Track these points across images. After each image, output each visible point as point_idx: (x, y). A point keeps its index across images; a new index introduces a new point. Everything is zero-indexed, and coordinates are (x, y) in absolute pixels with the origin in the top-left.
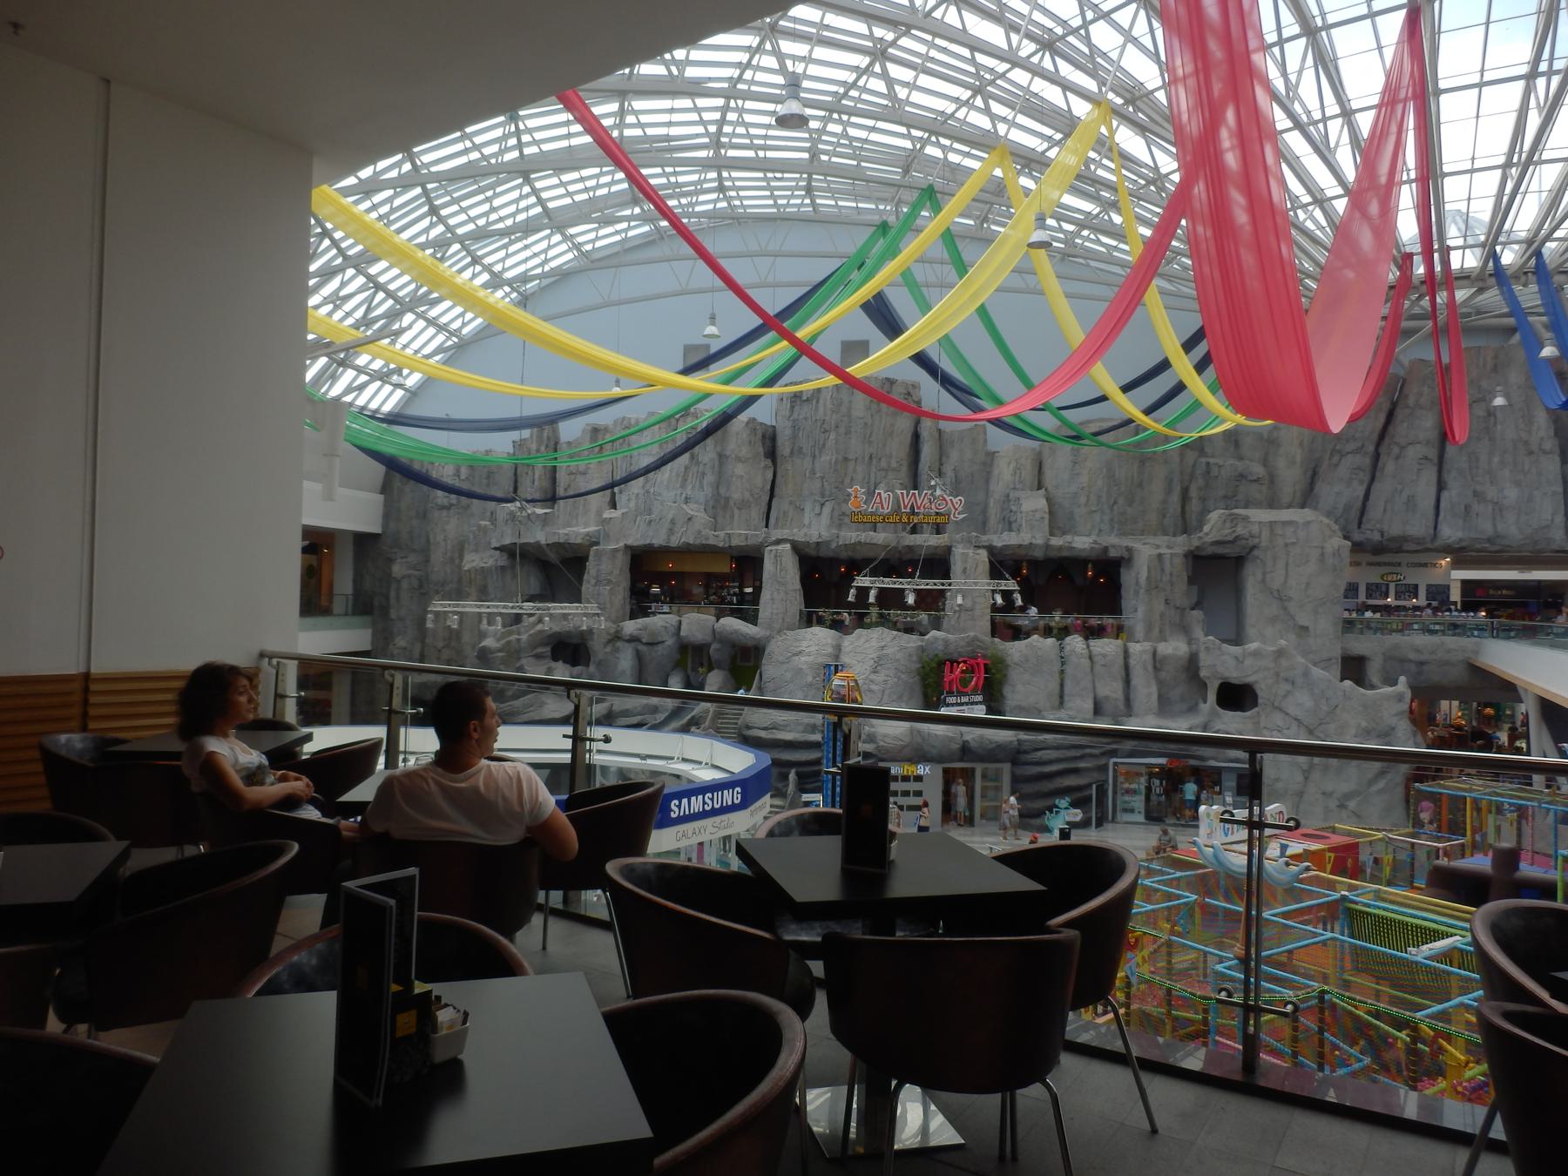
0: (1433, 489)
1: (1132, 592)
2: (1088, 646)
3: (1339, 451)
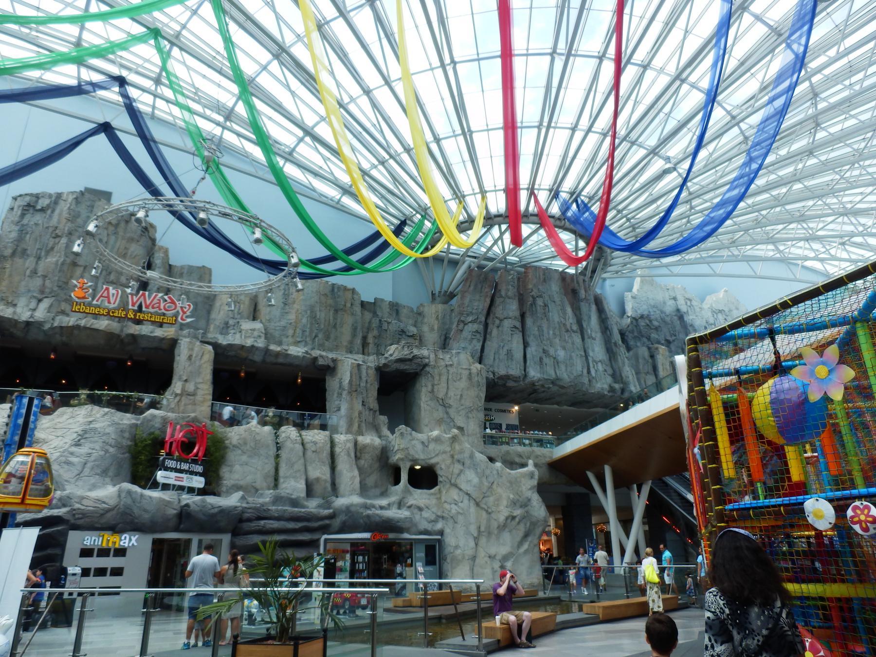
0: (521, 347)
1: (336, 395)
2: (301, 435)
3: (463, 322)
